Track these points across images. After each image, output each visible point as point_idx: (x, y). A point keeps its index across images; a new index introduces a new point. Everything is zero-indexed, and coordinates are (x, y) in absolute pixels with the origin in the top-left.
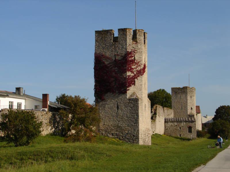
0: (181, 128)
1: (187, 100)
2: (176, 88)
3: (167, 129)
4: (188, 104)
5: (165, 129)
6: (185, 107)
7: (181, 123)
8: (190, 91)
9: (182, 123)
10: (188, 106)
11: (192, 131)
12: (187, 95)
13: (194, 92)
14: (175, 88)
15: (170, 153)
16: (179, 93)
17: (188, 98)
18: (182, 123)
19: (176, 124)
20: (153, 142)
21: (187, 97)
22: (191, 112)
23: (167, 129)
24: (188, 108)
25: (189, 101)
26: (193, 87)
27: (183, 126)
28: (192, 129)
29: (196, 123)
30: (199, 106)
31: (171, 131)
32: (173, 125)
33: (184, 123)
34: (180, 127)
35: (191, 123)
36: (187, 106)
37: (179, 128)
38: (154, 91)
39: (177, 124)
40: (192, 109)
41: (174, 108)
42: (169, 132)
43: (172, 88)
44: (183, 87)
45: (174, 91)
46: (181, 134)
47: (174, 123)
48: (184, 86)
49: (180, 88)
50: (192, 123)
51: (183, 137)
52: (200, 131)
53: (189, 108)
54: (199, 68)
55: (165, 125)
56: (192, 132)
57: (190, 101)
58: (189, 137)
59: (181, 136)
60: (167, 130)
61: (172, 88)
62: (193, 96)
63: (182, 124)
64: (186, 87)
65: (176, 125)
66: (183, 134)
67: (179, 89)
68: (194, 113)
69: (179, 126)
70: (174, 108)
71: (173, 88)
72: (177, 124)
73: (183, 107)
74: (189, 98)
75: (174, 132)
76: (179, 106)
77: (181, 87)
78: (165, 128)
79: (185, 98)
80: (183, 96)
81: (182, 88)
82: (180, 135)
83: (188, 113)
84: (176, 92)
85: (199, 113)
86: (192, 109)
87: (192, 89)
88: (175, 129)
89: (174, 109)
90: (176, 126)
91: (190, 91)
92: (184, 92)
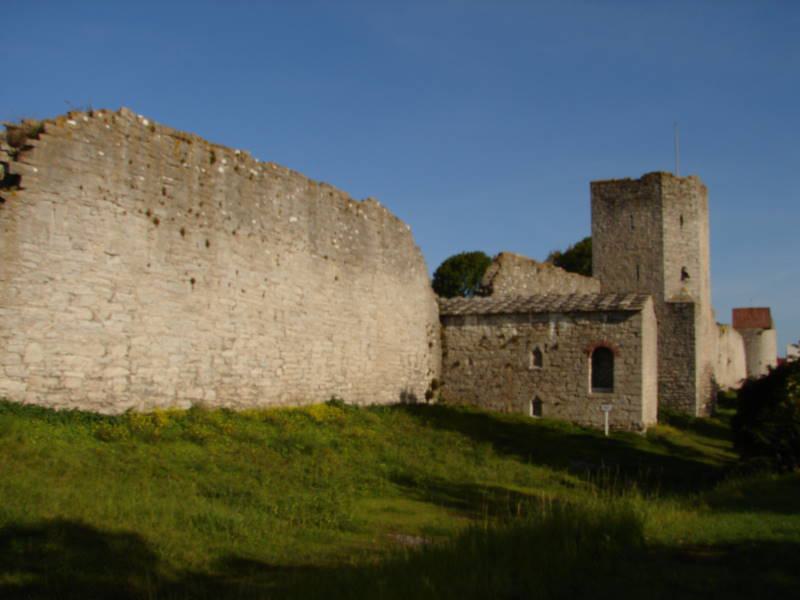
0: (545, 357)
1: (661, 234)
2: (613, 181)
4: (666, 254)
5: (444, 365)
6: (650, 267)
7: (546, 323)
8: (676, 191)
10: (666, 263)
13: (695, 196)
14: (606, 183)
16: (623, 204)
17: (665, 226)
18: (552, 325)
19: (511, 330)
20: (634, 399)
21: (661, 220)
22: (683, 290)
23: (457, 364)
24: (667, 273)
25: (669, 240)
26: (690, 178)
27: (556, 347)
28: (618, 363)
29: (640, 321)
31: (482, 377)
32: (495, 341)
33: (566, 325)
34: (537, 353)
35: (611, 321)
37: (532, 357)
39: (515, 332)
40: (685, 275)
41: (604, 271)
42: (471, 385)
43: (592, 184)
45: (602, 197)
46: (542, 397)
47: (500, 327)
48: (648, 171)
49: (628, 180)
51: (558, 417)
53: (671, 271)
54: (788, 278)
55: (443, 337)
56: (617, 385)
57: (675, 236)
58: (594, 418)
59: (545, 409)
61: (592, 184)
62: (692, 218)
63: (552, 331)
65: (514, 340)
66: (553, 400)
67: (624, 184)
69: (533, 347)
70: (604, 271)
71: (599, 184)
72: (515, 332)
73: (643, 269)
74: (669, 223)
75: (499, 386)
76: (626, 263)
77: (636, 174)
78: (445, 355)
79: (653, 224)
80: (643, 216)
81: (638, 181)
83: (669, 296)
84: (611, 202)
85: (769, 328)
86: (685, 275)
87: (684, 186)
88: (508, 365)
89: (603, 277)
90: (512, 346)
91: (676, 191)
92: (647, 197)
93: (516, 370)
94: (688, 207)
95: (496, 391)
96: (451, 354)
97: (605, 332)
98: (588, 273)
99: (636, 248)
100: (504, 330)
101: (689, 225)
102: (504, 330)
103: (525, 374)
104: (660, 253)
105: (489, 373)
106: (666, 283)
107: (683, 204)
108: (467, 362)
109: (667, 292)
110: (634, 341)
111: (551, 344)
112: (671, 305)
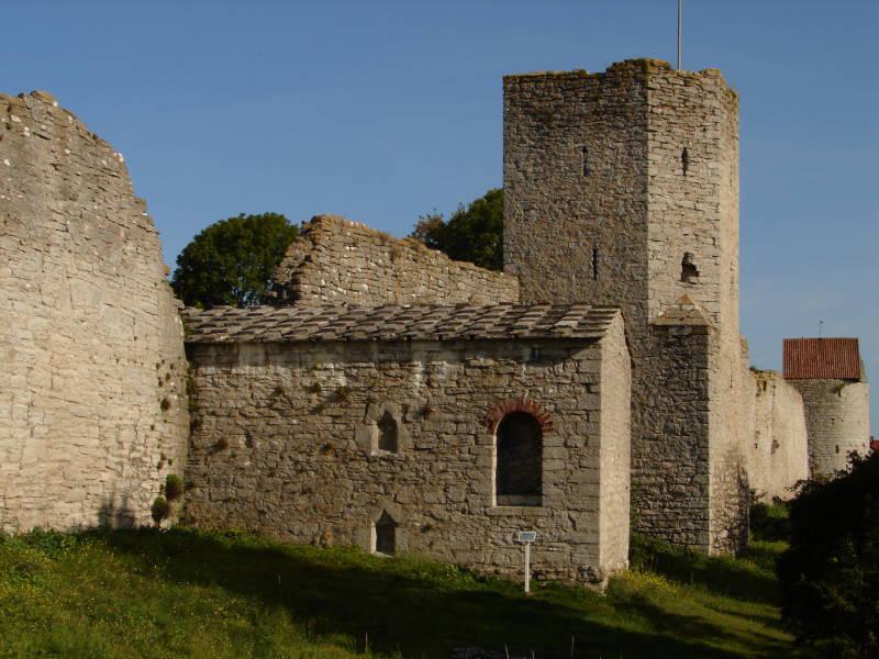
1: (645, 191)
2: (549, 76)
3: (221, 445)
5: (193, 447)
6: (620, 252)
7: (406, 363)
9: (419, 367)
10: (651, 245)
11: (547, 476)
12: (644, 142)
15: (56, 497)
16: (568, 125)
17: (652, 171)
18: (419, 367)
24: (653, 265)
25: (660, 199)
27: (425, 412)
28: (552, 445)
30: (855, 342)
32: (299, 398)
33: (446, 367)
34: (387, 424)
35: (536, 360)
36: (639, 244)
37: (376, 432)
38: (475, 199)
39: (342, 381)
40: (689, 270)
42: (249, 490)
43: (506, 79)
44: (615, 69)
46: (396, 513)
47: (310, 371)
49: (581, 75)
50: (554, 361)
52: (787, 552)
55: (192, 389)
56: (549, 490)
58: (501, 558)
60: (219, 461)
62: (708, 156)
64: (642, 64)
65: (340, 395)
66: (419, 520)
68: (711, 307)
69: (379, 411)
71: (522, 79)
74: (661, 164)
75: (306, 491)
78: (195, 426)
80: (608, 150)
81: (601, 77)
82: (387, 529)
83: (656, 312)
84: (545, 119)
85: (856, 380)
86: (689, 270)
87: (692, 90)
88: (326, 448)
90: (336, 409)
92: (617, 111)
93: (344, 458)
94: (698, 134)
95: (302, 501)
96: (209, 424)
97: (527, 383)
98: (495, 263)
99: (593, 214)
100: (321, 376)
101: (699, 170)
102: (321, 376)
103: (363, 466)
104: (642, 226)
105: (287, 465)
106: (651, 284)
107: (690, 128)
108: (242, 441)
109: (651, 303)
110: (584, 401)
111: (415, 405)
112: (662, 329)
